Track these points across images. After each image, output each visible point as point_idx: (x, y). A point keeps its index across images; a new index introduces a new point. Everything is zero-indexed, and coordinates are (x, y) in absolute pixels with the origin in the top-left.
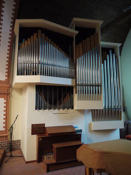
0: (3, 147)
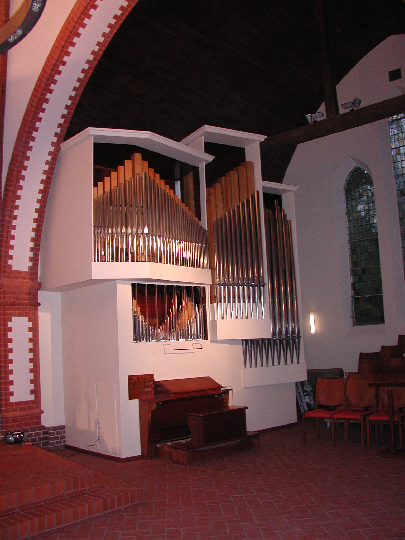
0: (35, 440)
